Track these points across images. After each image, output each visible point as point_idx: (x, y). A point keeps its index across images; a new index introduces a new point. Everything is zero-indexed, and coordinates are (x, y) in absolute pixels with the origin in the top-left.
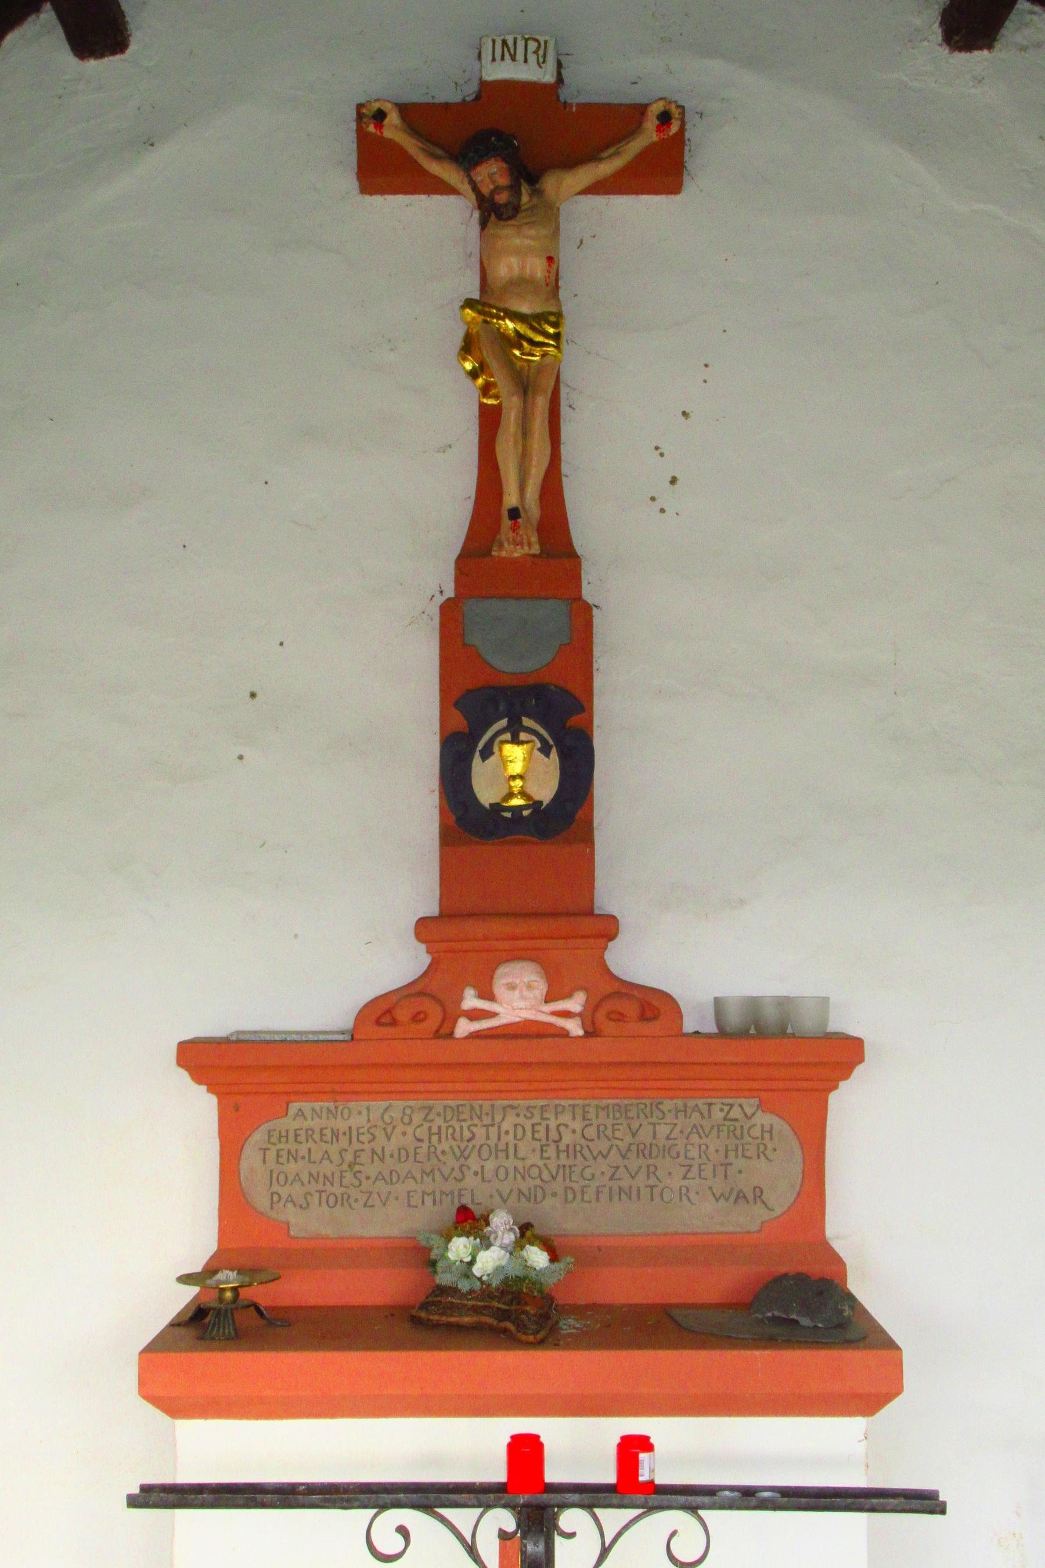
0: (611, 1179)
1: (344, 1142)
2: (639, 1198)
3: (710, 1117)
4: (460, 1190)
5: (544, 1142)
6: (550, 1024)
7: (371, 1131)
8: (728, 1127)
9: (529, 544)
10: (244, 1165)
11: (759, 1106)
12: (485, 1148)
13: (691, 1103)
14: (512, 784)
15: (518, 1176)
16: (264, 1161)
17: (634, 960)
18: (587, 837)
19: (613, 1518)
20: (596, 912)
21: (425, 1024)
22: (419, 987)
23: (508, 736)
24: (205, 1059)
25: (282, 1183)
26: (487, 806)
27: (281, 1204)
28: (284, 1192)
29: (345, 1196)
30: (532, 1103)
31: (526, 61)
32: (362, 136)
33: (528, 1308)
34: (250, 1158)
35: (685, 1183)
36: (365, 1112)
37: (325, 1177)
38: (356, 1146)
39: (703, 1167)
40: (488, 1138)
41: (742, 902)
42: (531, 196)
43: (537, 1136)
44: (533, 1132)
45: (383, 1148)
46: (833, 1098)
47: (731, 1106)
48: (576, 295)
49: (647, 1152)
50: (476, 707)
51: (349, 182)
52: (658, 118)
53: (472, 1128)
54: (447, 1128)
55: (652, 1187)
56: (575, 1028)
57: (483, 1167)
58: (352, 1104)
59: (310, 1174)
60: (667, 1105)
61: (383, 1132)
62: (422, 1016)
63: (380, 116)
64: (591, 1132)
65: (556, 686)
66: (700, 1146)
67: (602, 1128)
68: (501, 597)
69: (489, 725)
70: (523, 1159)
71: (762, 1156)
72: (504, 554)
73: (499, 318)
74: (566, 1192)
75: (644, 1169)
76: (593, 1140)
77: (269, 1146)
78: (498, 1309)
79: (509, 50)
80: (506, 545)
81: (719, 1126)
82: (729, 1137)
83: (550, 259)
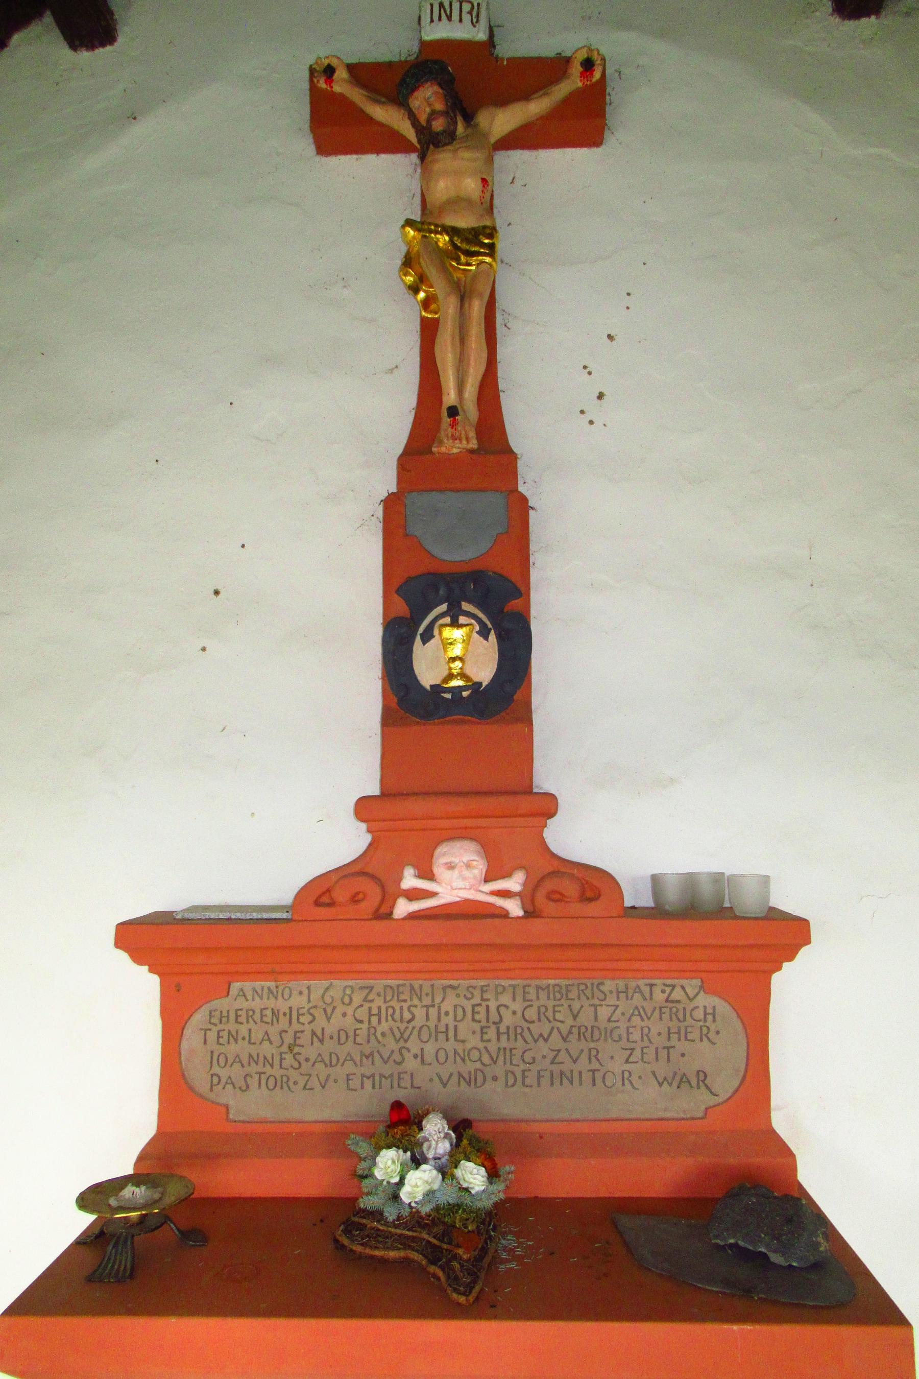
0: (552, 1063)
1: (284, 1022)
2: (581, 1084)
3: (651, 999)
4: (399, 1074)
5: (484, 1023)
6: (492, 905)
7: (311, 1011)
8: (671, 1009)
9: (468, 439)
10: (184, 1045)
11: (701, 987)
12: (425, 1028)
13: (633, 984)
14: (452, 665)
15: (458, 1058)
16: (205, 1042)
17: (575, 836)
18: (525, 717)
20: (535, 790)
21: (363, 905)
22: (357, 868)
23: (447, 620)
24: (142, 938)
25: (222, 1064)
26: (428, 688)
27: (220, 1086)
28: (224, 1073)
29: (285, 1079)
30: (474, 982)
31: (461, 20)
32: (313, 88)
33: (460, 1251)
34: (191, 1040)
35: (627, 1067)
36: (306, 992)
37: (265, 1058)
38: (296, 1026)
39: (645, 1050)
40: (428, 1019)
41: (672, 780)
42: (466, 128)
43: (477, 1017)
44: (474, 1013)
45: (323, 1029)
46: (776, 978)
47: (674, 987)
48: (510, 224)
49: (588, 1035)
50: (417, 595)
51: (305, 145)
52: (582, 64)
53: (413, 1009)
54: (387, 1008)
55: (594, 1071)
56: (514, 908)
57: (422, 1049)
58: (293, 984)
59: (250, 1056)
60: (609, 985)
61: (323, 1012)
62: (361, 896)
63: (329, 71)
64: (531, 1014)
65: (495, 573)
66: (642, 1029)
67: (543, 1010)
68: (440, 490)
69: (431, 609)
70: (463, 1041)
71: (705, 1039)
72: (443, 449)
73: (436, 233)
74: (507, 1075)
75: (586, 1052)
76: (533, 1022)
77: (210, 1026)
78: (428, 1242)
79: (445, 12)
80: (445, 441)
81: (661, 1008)
82: (671, 1019)
83: (484, 181)
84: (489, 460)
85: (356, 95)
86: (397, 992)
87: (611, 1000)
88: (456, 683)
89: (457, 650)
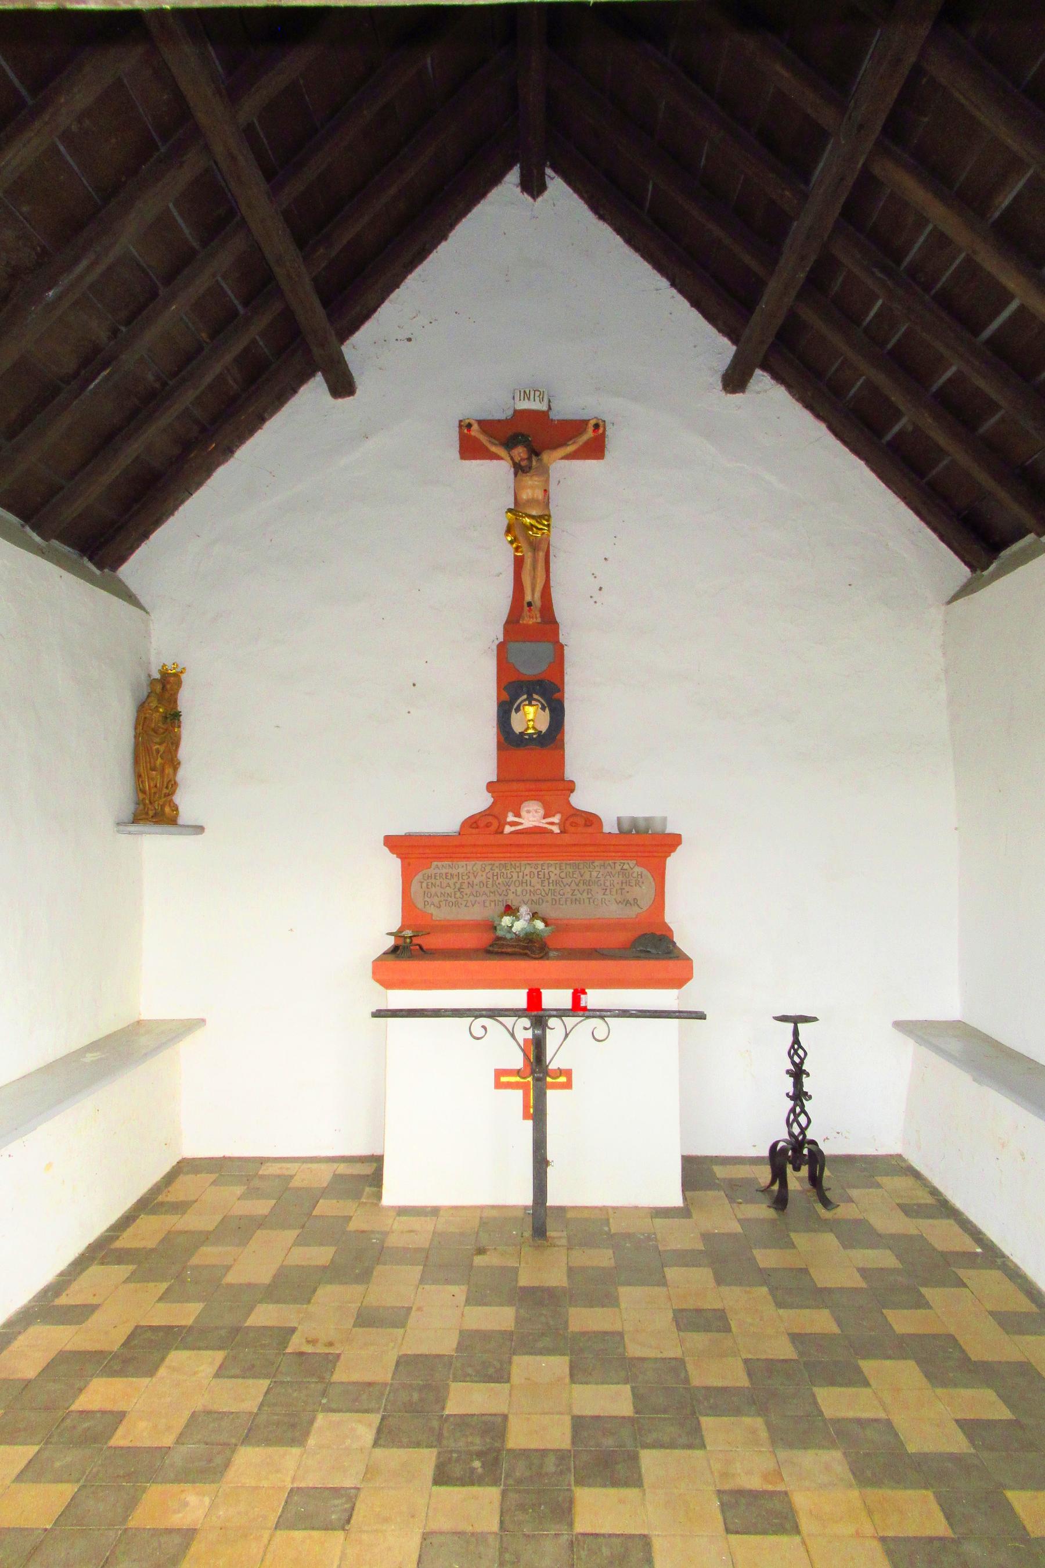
1: (456, 879)
17: (580, 800)
19: (570, 1021)
24: (393, 843)
32: (461, 433)
50: (513, 688)
56: (556, 830)
63: (469, 426)
64: (563, 875)
83: (545, 491)
84: (547, 626)
85: (483, 439)
86: (505, 866)
87: (597, 869)
88: (531, 731)
89: (531, 716)
